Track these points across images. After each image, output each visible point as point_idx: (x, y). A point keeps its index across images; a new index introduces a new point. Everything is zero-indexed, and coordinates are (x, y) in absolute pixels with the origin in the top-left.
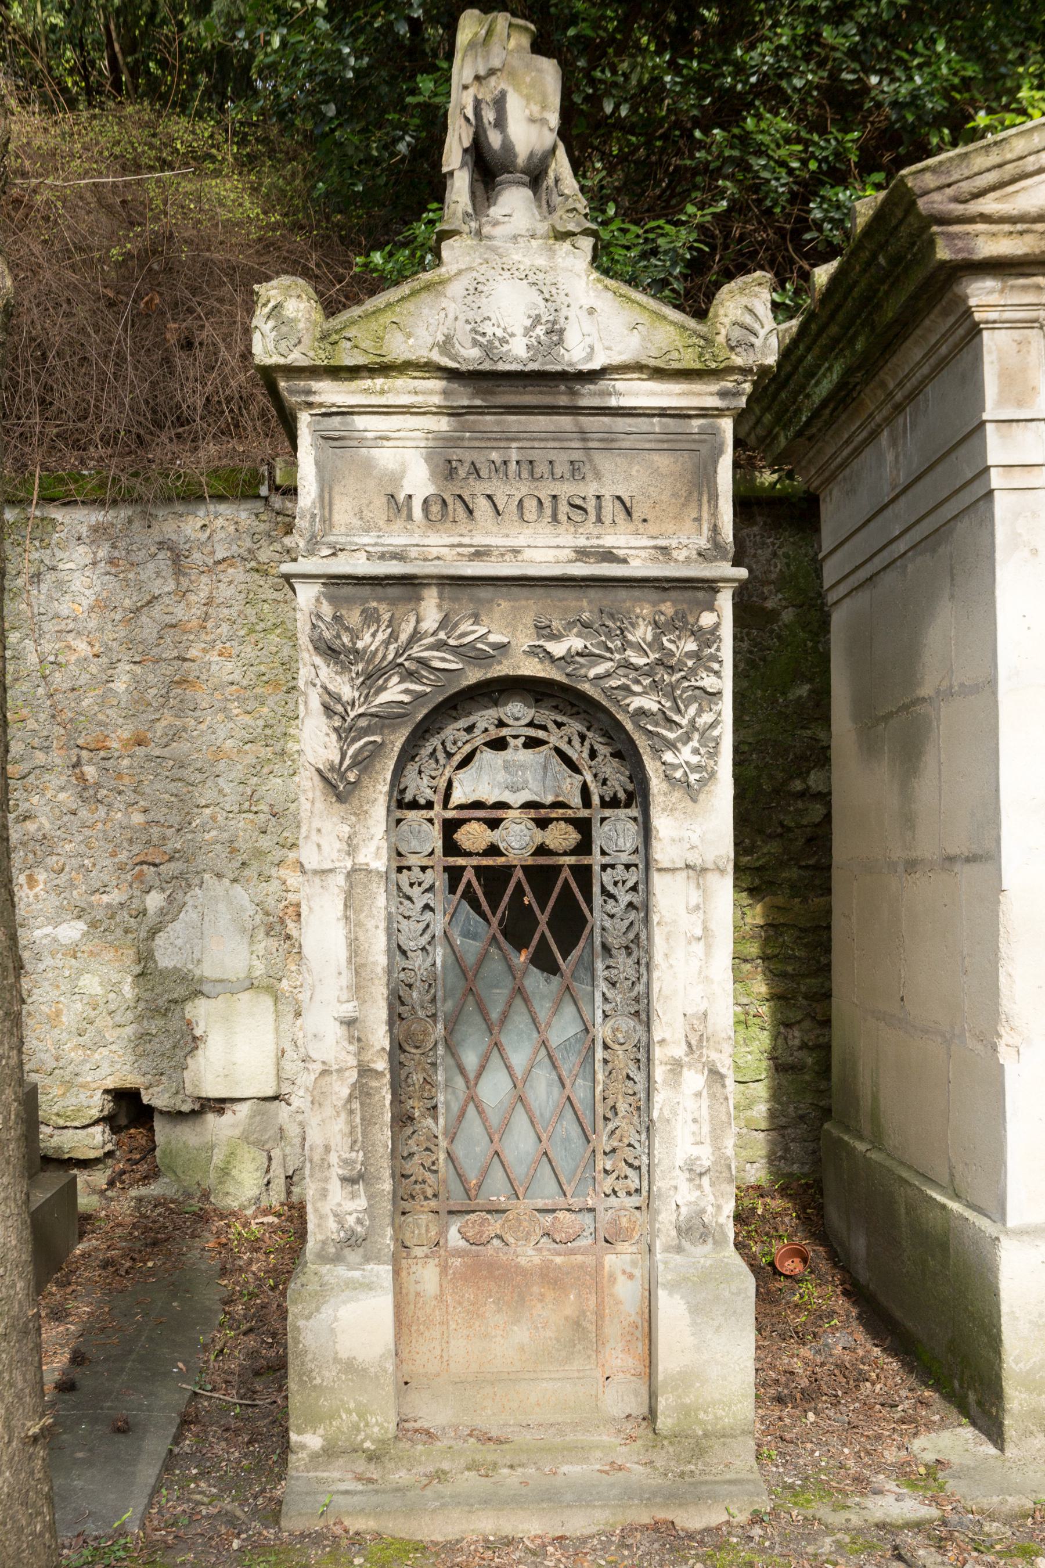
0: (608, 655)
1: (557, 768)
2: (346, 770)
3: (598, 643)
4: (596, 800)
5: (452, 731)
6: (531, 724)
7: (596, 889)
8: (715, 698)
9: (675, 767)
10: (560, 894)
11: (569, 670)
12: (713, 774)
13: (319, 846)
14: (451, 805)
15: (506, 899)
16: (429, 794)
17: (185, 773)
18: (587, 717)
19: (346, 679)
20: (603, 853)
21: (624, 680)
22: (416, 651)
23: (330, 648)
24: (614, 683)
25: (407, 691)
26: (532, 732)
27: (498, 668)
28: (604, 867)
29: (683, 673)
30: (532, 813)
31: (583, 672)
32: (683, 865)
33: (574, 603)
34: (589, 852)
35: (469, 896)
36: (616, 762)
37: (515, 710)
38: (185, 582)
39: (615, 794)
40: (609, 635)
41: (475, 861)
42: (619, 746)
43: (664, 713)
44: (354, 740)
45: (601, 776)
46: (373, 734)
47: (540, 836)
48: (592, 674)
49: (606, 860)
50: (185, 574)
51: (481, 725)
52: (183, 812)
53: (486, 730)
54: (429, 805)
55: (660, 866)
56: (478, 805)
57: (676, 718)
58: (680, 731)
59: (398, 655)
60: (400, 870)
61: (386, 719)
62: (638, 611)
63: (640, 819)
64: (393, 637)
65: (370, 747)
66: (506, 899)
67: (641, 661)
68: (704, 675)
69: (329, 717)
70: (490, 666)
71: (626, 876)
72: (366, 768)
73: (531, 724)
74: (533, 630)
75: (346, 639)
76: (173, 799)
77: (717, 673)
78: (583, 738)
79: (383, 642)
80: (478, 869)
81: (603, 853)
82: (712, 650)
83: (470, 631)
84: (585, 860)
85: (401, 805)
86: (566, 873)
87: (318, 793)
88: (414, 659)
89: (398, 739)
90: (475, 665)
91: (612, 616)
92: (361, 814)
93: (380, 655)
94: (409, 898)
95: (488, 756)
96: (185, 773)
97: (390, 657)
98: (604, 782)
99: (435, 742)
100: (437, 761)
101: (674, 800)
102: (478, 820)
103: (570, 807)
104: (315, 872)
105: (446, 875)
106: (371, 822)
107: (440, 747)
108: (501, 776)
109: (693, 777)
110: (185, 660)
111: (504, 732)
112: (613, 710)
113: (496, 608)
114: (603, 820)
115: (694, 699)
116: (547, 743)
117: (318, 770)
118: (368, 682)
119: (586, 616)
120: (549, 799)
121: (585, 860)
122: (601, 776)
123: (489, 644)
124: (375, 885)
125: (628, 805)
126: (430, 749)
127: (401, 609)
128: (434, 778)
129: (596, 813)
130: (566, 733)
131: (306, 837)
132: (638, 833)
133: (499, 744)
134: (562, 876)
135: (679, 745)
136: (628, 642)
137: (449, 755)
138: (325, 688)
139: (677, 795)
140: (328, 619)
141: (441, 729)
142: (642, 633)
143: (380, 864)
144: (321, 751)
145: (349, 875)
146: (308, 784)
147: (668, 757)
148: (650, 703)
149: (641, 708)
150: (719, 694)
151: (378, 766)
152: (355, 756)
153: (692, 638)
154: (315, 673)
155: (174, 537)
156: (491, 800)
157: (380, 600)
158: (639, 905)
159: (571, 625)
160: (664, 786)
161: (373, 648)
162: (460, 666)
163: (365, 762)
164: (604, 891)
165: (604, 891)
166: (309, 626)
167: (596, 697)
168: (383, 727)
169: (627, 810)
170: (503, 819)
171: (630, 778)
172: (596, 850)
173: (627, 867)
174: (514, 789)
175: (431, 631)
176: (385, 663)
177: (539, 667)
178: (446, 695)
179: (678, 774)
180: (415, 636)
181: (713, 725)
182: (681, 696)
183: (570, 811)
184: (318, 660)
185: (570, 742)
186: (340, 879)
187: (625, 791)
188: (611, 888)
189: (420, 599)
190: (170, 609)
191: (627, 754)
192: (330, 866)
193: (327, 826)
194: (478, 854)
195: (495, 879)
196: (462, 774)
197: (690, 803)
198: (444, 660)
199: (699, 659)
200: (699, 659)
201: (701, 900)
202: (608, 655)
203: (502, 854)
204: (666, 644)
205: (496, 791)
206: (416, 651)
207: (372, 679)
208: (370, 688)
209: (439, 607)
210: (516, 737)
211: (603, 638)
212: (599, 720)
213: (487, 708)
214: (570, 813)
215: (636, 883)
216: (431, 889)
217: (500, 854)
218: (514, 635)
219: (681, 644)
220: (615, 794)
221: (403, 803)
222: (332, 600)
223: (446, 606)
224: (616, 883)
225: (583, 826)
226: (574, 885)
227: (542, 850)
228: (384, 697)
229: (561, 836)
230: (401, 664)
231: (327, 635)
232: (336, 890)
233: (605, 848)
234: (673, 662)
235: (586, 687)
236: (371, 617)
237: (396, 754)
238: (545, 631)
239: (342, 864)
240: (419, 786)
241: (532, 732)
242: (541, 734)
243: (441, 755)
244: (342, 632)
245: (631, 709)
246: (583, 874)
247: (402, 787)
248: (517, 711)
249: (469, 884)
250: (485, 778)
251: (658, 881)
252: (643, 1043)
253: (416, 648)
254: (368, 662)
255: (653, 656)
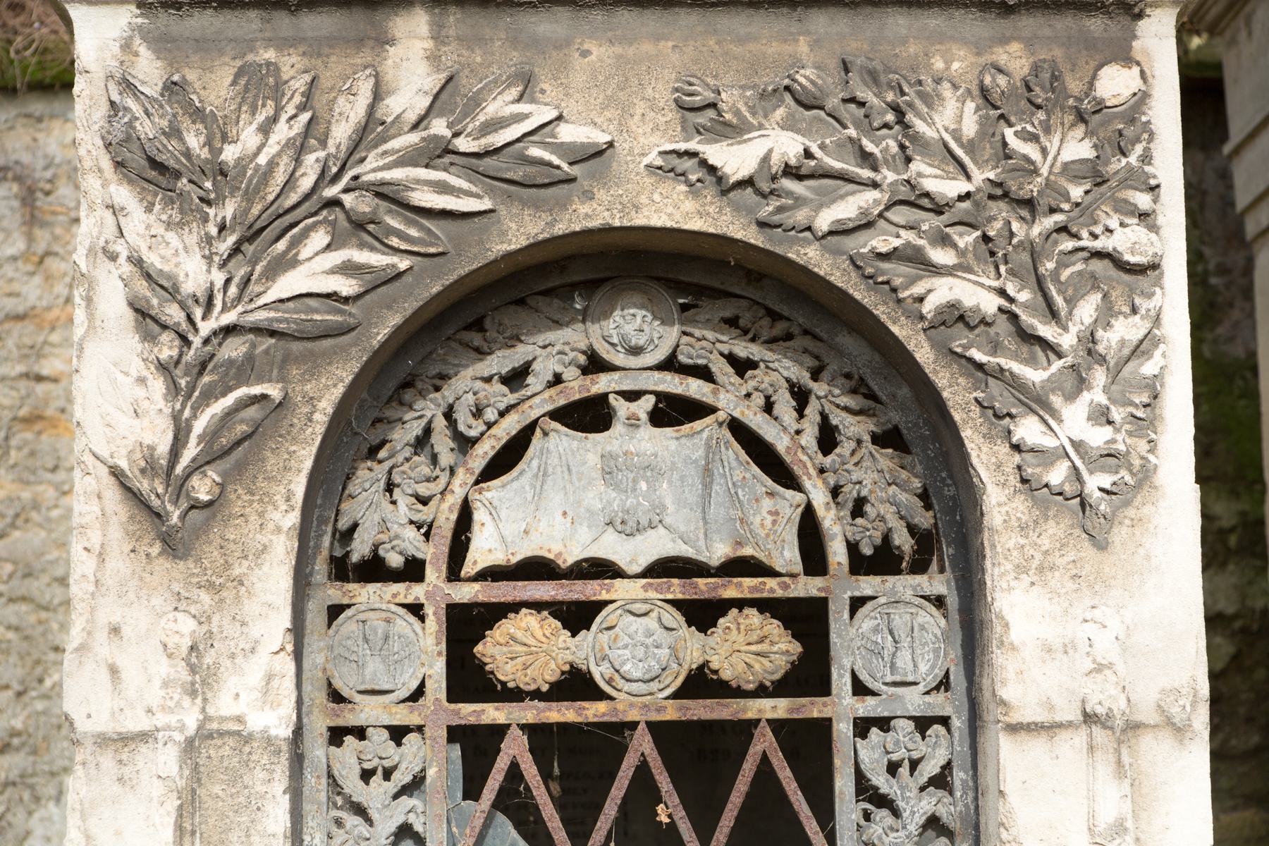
0: (866, 173)
1: (738, 474)
2: (188, 476)
3: (839, 145)
4: (837, 553)
5: (471, 382)
6: (670, 364)
7: (844, 784)
8: (1142, 282)
9: (1046, 456)
10: (749, 796)
11: (767, 210)
12: (1145, 475)
13: (114, 671)
14: (469, 569)
15: (610, 810)
16: (411, 541)
17: (35, 587)
18: (807, 342)
19: (192, 239)
20: (860, 689)
21: (908, 236)
22: (372, 168)
23: (155, 164)
24: (882, 242)
25: (348, 269)
26: (673, 384)
27: (584, 209)
28: (863, 727)
29: (1059, 218)
30: (676, 588)
31: (801, 216)
32: (1076, 716)
33: (774, 49)
34: (823, 687)
35: (514, 802)
36: (885, 459)
37: (629, 329)
38: (43, 238)
39: (886, 538)
40: (868, 125)
41: (531, 712)
42: (895, 417)
43: (1014, 317)
44: (209, 396)
45: (850, 493)
46: (260, 380)
47: (695, 648)
48: (824, 221)
49: (868, 706)
50: (44, 224)
51: (544, 368)
52: (29, 661)
53: (557, 380)
54: (413, 570)
55: (1014, 718)
56: (537, 569)
57: (1046, 331)
58: (1057, 364)
59: (325, 178)
60: (337, 735)
61: (296, 338)
62: (939, 64)
63: (953, 602)
64: (313, 133)
65: (253, 412)
66: (610, 810)
67: (948, 187)
68: (1113, 223)
69: (148, 337)
70: (563, 205)
71: (920, 748)
72: (240, 467)
73: (670, 364)
74: (672, 115)
75: (194, 141)
76: (11, 635)
77: (1144, 216)
78: (801, 397)
79: (289, 143)
80: (535, 731)
81: (860, 689)
82: (1133, 159)
83: (508, 114)
84: (814, 708)
85: (342, 570)
86: (764, 742)
87: (116, 533)
88: (367, 187)
89: (326, 392)
90: (524, 203)
91: (873, 77)
92: (225, 586)
93: (280, 177)
94: (360, 810)
95: (560, 443)
96: (35, 587)
97: (306, 183)
98: (858, 509)
99: (429, 408)
100: (434, 459)
101: (1046, 543)
102: (537, 606)
103: (771, 573)
104: (103, 741)
105: (456, 751)
106: (251, 608)
107: (440, 423)
108: (597, 496)
109: (1095, 482)
110: (39, 378)
111: (602, 383)
112: (881, 312)
113: (577, 62)
114: (857, 603)
115: (1094, 282)
116: (712, 410)
117: (116, 473)
118: (249, 249)
119: (805, 77)
120: (718, 553)
121: (814, 708)
122: (850, 493)
123: (560, 149)
124: (260, 775)
125: (919, 567)
126: (416, 429)
127: (333, 68)
128: (424, 501)
129: (839, 586)
130: (762, 387)
131: (82, 648)
132: (946, 637)
133: (589, 416)
134: (756, 749)
135: (1056, 400)
136: (916, 138)
137: (465, 443)
138: (138, 262)
139: (1054, 530)
140: (152, 90)
141: (444, 377)
142: (954, 117)
143: (276, 721)
144: (125, 422)
145: (190, 747)
146: (94, 511)
147: (1029, 430)
148: (977, 295)
149: (953, 305)
150: (1151, 268)
151: (272, 462)
152: (210, 436)
153: (1080, 130)
154: (113, 222)
155: (26, 158)
156: (570, 556)
157: (283, 44)
158: (954, 825)
159: (770, 97)
160: (1021, 507)
161: (262, 160)
162: (486, 204)
163: (237, 450)
164: (864, 789)
165: (864, 789)
166: (104, 108)
167: (837, 279)
168: (286, 360)
169: (918, 579)
170: (601, 605)
171: (924, 496)
172: (841, 682)
173: (923, 724)
174: (628, 528)
175: (412, 117)
176: (293, 198)
177: (689, 205)
178: (452, 278)
179: (1057, 475)
180: (371, 130)
181: (1140, 350)
182: (1055, 274)
183: (771, 583)
184: (123, 194)
185: (768, 407)
186: (165, 760)
187: (912, 529)
188: (881, 781)
189: (384, 41)
190: (16, 287)
191: (919, 431)
192: (135, 722)
193: (136, 619)
194: (536, 695)
195: (582, 757)
196: (495, 490)
197: (1088, 551)
198: (443, 188)
199: (1100, 181)
200: (1100, 181)
201: (1127, 807)
202: (866, 173)
203: (600, 695)
204: (1014, 143)
205: (584, 534)
206: (372, 168)
207: (260, 237)
208: (253, 262)
209: (434, 59)
210: (632, 396)
211: (852, 132)
212: (840, 353)
213: (558, 324)
214: (772, 587)
215: (948, 766)
216: (415, 785)
217: (597, 694)
218: (623, 128)
219: (1053, 144)
220: (886, 538)
221: (340, 564)
222: (161, 44)
223: (451, 56)
224: (893, 768)
225: (807, 620)
226: (785, 774)
227: (701, 683)
228: (289, 284)
229: (749, 648)
230: (335, 203)
231: (146, 128)
232: (158, 789)
233: (863, 676)
234: (1033, 188)
235: (810, 255)
236: (259, 86)
237: (320, 429)
238: (702, 114)
239: (172, 719)
240: (385, 518)
241: (673, 384)
242: (694, 388)
243: (442, 443)
244: (185, 123)
245: (928, 308)
246: (809, 745)
247: (344, 524)
248: (635, 331)
249: (514, 772)
250: (555, 500)
251: (1013, 760)
252: (160, 147)
253: (372, 161)
254: (249, 197)
255: (981, 176)
